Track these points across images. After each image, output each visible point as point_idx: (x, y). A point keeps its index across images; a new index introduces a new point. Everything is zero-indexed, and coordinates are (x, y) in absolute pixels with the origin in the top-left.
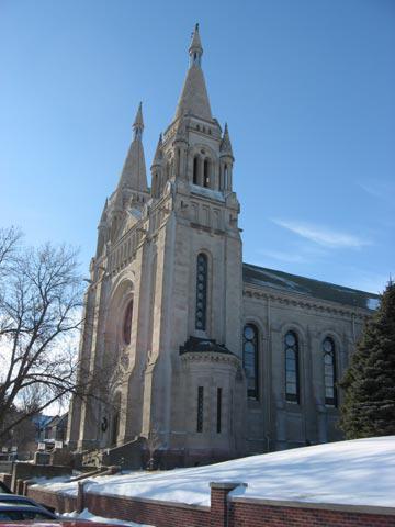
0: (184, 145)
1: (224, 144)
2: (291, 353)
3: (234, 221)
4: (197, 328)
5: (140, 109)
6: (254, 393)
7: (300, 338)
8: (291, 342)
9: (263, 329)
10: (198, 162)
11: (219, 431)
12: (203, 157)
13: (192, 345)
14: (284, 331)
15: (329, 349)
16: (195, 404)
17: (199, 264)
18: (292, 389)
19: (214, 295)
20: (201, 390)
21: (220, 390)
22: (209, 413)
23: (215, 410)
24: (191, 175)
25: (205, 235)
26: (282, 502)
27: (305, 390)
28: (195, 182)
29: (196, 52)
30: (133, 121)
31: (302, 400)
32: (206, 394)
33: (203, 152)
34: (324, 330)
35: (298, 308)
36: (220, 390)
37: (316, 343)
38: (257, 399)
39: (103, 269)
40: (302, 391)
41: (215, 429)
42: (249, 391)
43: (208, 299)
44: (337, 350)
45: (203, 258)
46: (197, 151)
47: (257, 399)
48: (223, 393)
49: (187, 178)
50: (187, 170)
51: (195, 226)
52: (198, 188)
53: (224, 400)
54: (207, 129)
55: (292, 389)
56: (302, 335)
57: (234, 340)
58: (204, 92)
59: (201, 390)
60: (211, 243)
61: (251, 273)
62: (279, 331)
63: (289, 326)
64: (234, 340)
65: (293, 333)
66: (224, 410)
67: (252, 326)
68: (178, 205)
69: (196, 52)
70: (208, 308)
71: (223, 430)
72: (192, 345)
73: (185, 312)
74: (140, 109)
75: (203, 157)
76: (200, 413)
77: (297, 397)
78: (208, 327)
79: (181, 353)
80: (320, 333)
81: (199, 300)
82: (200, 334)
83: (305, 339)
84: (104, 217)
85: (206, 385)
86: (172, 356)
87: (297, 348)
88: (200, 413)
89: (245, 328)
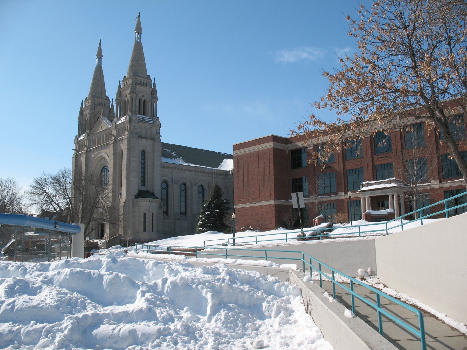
0: (135, 95)
1: (154, 92)
2: (183, 193)
4: (141, 185)
5: (100, 44)
6: (166, 213)
7: (187, 186)
8: (183, 188)
9: (170, 183)
11: (152, 231)
12: (143, 99)
13: (141, 194)
14: (180, 183)
16: (142, 220)
17: (142, 155)
18: (183, 210)
19: (148, 170)
20: (145, 214)
21: (153, 214)
22: (148, 224)
23: (151, 226)
24: (137, 109)
25: (144, 141)
27: (189, 211)
28: (139, 113)
29: (139, 30)
30: (96, 52)
31: (188, 215)
32: (147, 216)
33: (143, 96)
35: (187, 172)
36: (153, 214)
37: (195, 190)
38: (167, 215)
39: (86, 146)
40: (188, 211)
41: (151, 230)
42: (164, 211)
43: (146, 172)
45: (143, 153)
46: (140, 95)
47: (167, 215)
49: (136, 114)
50: (136, 107)
51: (140, 137)
52: (141, 116)
54: (145, 82)
55: (183, 210)
56: (188, 184)
57: (158, 190)
59: (145, 214)
60: (146, 144)
61: (165, 145)
63: (182, 181)
64: (158, 190)
65: (184, 184)
66: (155, 222)
67: (166, 182)
68: (132, 127)
69: (139, 30)
71: (154, 230)
72: (141, 194)
73: (137, 180)
74: (100, 44)
75: (143, 99)
76: (145, 224)
77: (185, 214)
78: (146, 185)
79: (136, 198)
81: (142, 172)
82: (143, 188)
84: (81, 113)
85: (147, 212)
88: (145, 224)
89: (162, 183)
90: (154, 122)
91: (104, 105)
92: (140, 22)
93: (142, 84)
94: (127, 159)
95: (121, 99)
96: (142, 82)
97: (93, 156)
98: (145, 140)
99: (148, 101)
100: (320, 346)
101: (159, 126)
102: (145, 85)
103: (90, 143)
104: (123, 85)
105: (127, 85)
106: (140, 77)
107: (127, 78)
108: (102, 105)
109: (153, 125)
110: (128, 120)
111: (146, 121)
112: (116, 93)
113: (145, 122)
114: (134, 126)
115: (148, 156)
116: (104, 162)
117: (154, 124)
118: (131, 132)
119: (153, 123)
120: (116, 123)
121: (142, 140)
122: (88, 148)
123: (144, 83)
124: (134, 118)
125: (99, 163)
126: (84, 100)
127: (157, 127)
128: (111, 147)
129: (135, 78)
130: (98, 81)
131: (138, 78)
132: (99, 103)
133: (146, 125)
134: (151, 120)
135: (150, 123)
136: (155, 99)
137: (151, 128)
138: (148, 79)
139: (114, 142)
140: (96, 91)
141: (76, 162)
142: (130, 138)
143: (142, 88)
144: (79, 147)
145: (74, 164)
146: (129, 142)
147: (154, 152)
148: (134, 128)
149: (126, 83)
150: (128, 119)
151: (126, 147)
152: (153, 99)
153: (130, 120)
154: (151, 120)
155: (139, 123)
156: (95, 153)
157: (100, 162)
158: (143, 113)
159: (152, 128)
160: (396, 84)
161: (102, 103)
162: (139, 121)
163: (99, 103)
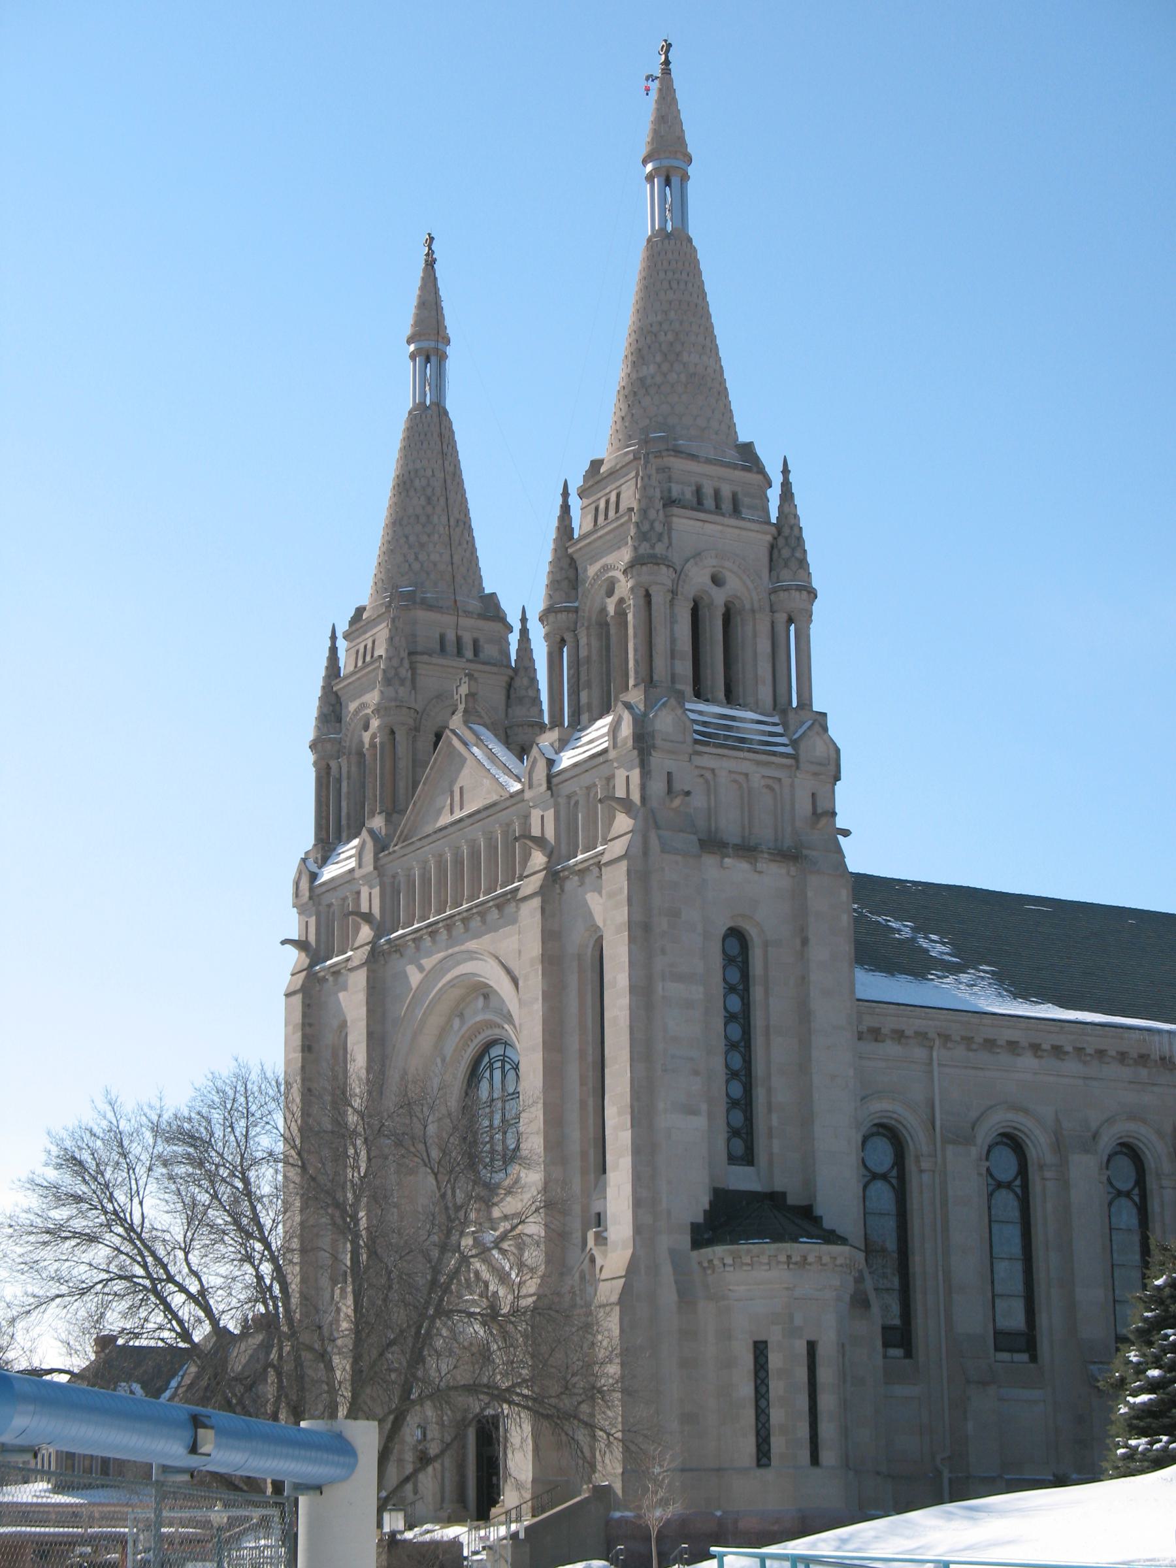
2: (1007, 1203)
3: (824, 813)
4: (732, 1159)
5: (430, 263)
7: (1032, 1153)
10: (704, 613)
11: (815, 1460)
12: (719, 597)
15: (1126, 1184)
16: (746, 1389)
17: (729, 960)
20: (760, 1350)
21: (812, 1347)
24: (685, 668)
25: (738, 868)
26: (606, 1221)
27: (1050, 1320)
28: (698, 694)
30: (405, 318)
32: (775, 1360)
33: (717, 580)
34: (1110, 1121)
35: (1028, 1061)
36: (812, 1347)
40: (1043, 1320)
41: (805, 1455)
42: (885, 1329)
43: (759, 1069)
44: (1151, 1183)
46: (698, 578)
48: (822, 1351)
49: (680, 697)
50: (673, 654)
51: (713, 844)
53: (826, 1375)
56: (1039, 1146)
58: (709, 346)
59: (760, 1350)
62: (967, 1139)
63: (999, 1120)
65: (1012, 1141)
66: (827, 1401)
68: (658, 786)
70: (760, 1095)
71: (828, 1456)
73: (700, 1122)
75: (719, 597)
79: (697, 1244)
80: (1095, 1136)
82: (743, 1180)
83: (1049, 1158)
85: (774, 1336)
86: (672, 1252)
87: (1025, 1186)
90: (794, 743)
91: (469, 654)
93: (709, 503)
94: (633, 989)
95: (576, 610)
96: (708, 491)
97: (415, 977)
98: (744, 866)
99: (753, 611)
102: (727, 506)
103: (391, 894)
105: (612, 513)
106: (693, 457)
107: (613, 473)
108: (460, 652)
110: (630, 743)
111: (743, 740)
112: (545, 569)
114: (669, 774)
117: (795, 757)
119: (789, 750)
122: (380, 930)
125: (457, 1022)
128: (530, 915)
130: (429, 500)
131: (679, 465)
132: (442, 638)
133: (745, 767)
134: (779, 729)
140: (416, 566)
141: (310, 1025)
142: (646, 853)
143: (709, 528)
144: (325, 926)
147: (805, 942)
148: (670, 790)
150: (626, 730)
152: (782, 594)
153: (643, 741)
154: (779, 729)
158: (721, 695)
159: (786, 782)
162: (696, 742)
163: (442, 638)
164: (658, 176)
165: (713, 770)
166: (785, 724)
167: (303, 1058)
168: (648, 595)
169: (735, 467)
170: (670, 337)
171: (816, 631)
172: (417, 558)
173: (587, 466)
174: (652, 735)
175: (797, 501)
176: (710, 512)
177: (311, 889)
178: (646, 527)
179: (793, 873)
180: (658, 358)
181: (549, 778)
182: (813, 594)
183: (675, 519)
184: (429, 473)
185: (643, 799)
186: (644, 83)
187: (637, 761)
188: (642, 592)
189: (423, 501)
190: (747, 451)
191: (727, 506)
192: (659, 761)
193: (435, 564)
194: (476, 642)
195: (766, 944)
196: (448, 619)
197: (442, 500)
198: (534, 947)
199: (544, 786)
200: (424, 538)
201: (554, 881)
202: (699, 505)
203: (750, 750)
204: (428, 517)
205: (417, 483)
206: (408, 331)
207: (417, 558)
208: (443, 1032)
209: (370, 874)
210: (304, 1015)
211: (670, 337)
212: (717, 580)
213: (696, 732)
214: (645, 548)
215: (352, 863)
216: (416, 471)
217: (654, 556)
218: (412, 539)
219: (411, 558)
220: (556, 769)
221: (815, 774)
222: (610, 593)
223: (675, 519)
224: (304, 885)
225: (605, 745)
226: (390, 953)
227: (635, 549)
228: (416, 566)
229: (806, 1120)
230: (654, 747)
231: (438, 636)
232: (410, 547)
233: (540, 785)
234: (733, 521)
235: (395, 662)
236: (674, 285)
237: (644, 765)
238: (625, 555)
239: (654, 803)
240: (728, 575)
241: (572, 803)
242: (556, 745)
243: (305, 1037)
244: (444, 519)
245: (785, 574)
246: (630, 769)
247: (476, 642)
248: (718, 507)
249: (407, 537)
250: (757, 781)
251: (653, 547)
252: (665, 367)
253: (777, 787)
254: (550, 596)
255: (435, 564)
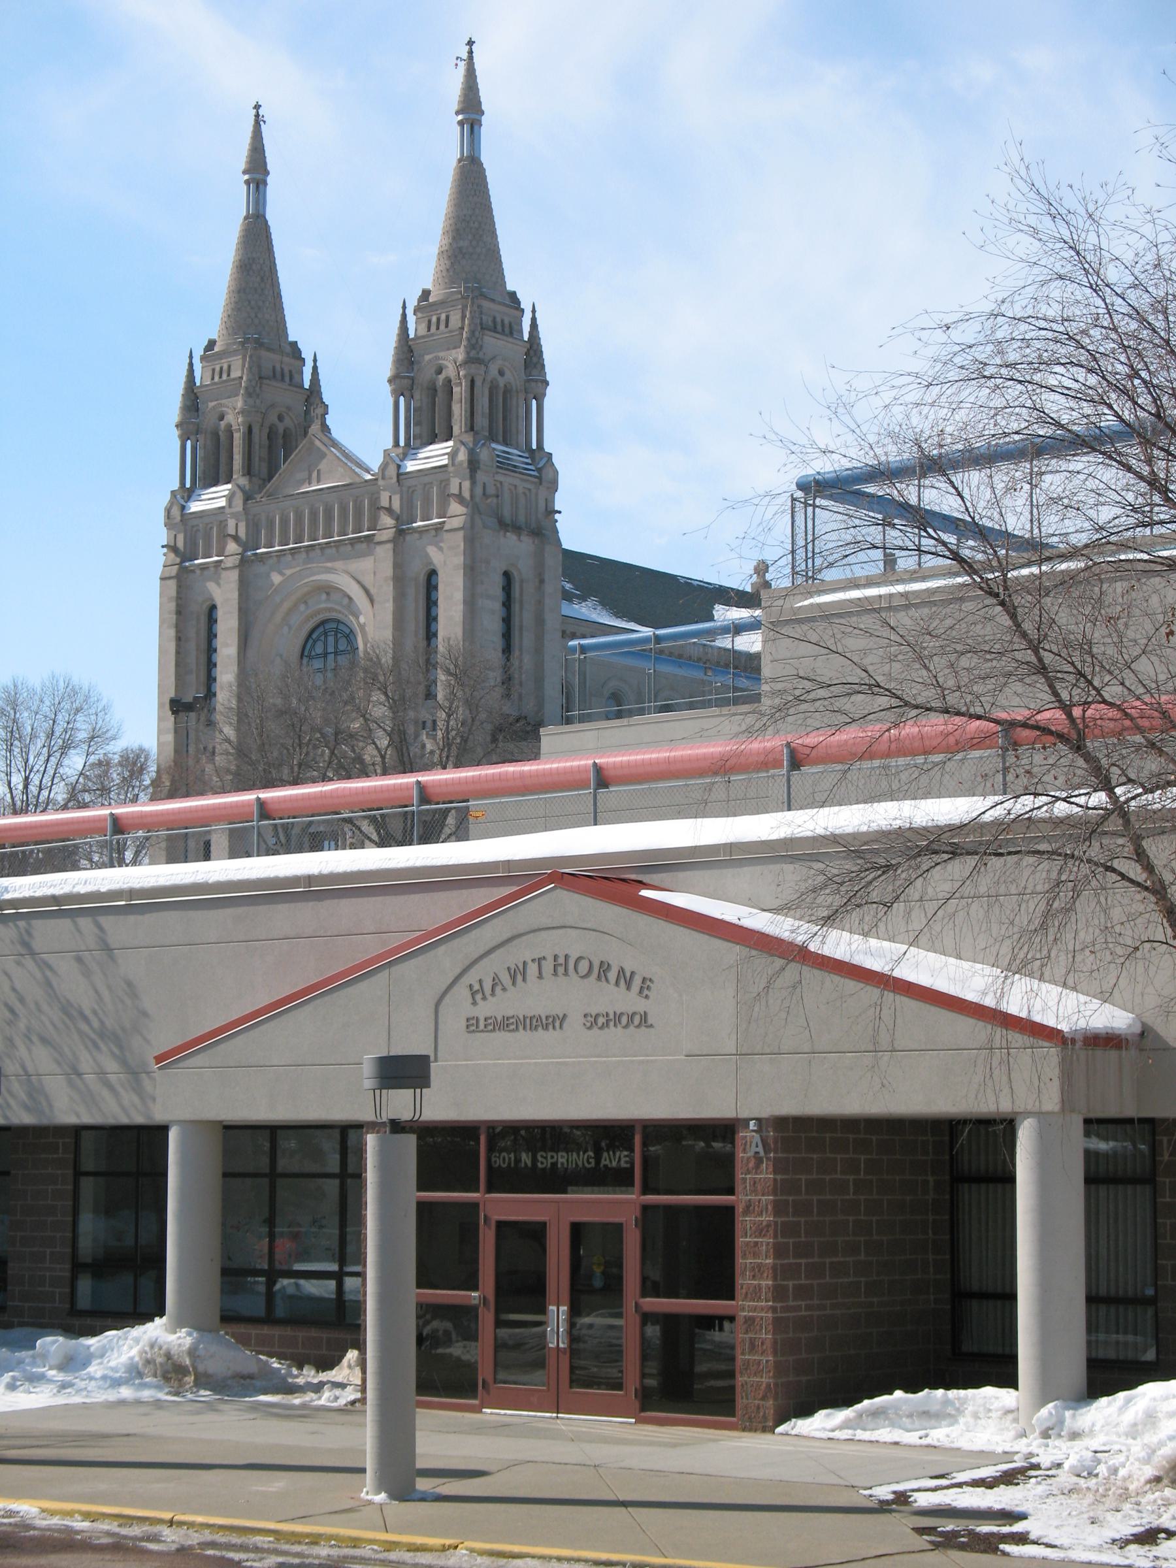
1: (533, 353)
12: (501, 382)
25: (512, 537)
33: (501, 373)
61: (568, 554)
68: (479, 490)
74: (258, 120)
75: (501, 382)
90: (539, 470)
91: (287, 379)
92: (474, 70)
93: (499, 328)
94: (465, 602)
95: (412, 379)
96: (498, 320)
97: (276, 578)
98: (514, 537)
99: (517, 392)
100: (1066, 1491)
101: (553, 486)
102: (507, 330)
103: (254, 527)
104: (424, 326)
105: (442, 326)
106: (493, 300)
107: (442, 303)
108: (283, 380)
109: (536, 480)
110: (466, 465)
111: (515, 466)
112: (391, 352)
113: (516, 472)
114: (484, 484)
115: (521, 595)
116: (329, 605)
117: (540, 478)
118: (474, 508)
119: (535, 473)
120: (399, 467)
121: (505, 536)
122: (246, 546)
123: (502, 321)
124: (484, 455)
125: (302, 607)
126: (198, 352)
127: (548, 488)
128: (384, 555)
129: (479, 306)
130: (262, 279)
131: (486, 304)
132: (274, 368)
133: (517, 482)
134: (529, 461)
135: (530, 475)
136: (540, 384)
137: (530, 490)
138: (511, 307)
139: (394, 538)
140: (256, 321)
141: (181, 598)
142: (473, 526)
143: (500, 343)
144: (191, 542)
145: (172, 606)
146: (471, 541)
147: (542, 581)
148: (484, 494)
149: (434, 319)
150: (462, 456)
151: (460, 560)
152: (533, 384)
153: (473, 465)
154: (529, 461)
155: (497, 473)
156: (288, 572)
157: (306, 603)
158: (501, 439)
159: (534, 491)
160: (1116, 741)
161: (282, 369)
162: (498, 467)
163: (274, 368)
164: (467, 123)
165: (501, 483)
166: (533, 459)
167: (177, 619)
168: (472, 382)
169: (507, 306)
170: (476, 225)
171: (548, 402)
172: (256, 316)
173: (420, 293)
174: (478, 462)
175: (539, 329)
176: (507, 336)
177: (182, 515)
178: (474, 341)
179: (536, 541)
180: (470, 237)
181: (399, 475)
182: (547, 383)
183: (485, 337)
184: (262, 262)
185: (472, 496)
186: (455, 62)
187: (468, 476)
188: (470, 378)
189: (258, 279)
190: (513, 296)
191: (507, 330)
192: (481, 476)
193: (268, 321)
194: (290, 372)
195: (522, 581)
196: (276, 357)
197: (270, 281)
198: (387, 569)
199: (395, 479)
200: (260, 303)
201: (400, 535)
202: (495, 330)
203: (520, 473)
204: (262, 290)
205: (254, 267)
206: (243, 166)
207: (256, 316)
208: (290, 611)
209: (238, 512)
210: (178, 593)
211: (476, 225)
212: (501, 373)
213: (498, 462)
214: (473, 353)
215: (222, 503)
216: (254, 259)
217: (479, 359)
218: (253, 303)
219: (253, 315)
220: (401, 471)
221: (548, 488)
222: (439, 371)
223: (485, 337)
224: (176, 512)
225: (445, 462)
226: (252, 561)
227: (468, 353)
228: (256, 321)
229: (539, 681)
230: (479, 468)
231: (271, 368)
232: (252, 308)
233: (391, 478)
234: (510, 340)
235: (253, 383)
236: (477, 193)
237: (473, 478)
238: (460, 354)
239: (477, 499)
240: (506, 369)
241: (411, 490)
242: (401, 456)
243: (178, 605)
244: (271, 292)
245: (535, 372)
246: (464, 479)
247: (290, 372)
248: (503, 330)
249: (249, 302)
250: (520, 490)
251: (478, 353)
252: (474, 243)
253: (528, 494)
254: (397, 368)
255: (268, 321)
